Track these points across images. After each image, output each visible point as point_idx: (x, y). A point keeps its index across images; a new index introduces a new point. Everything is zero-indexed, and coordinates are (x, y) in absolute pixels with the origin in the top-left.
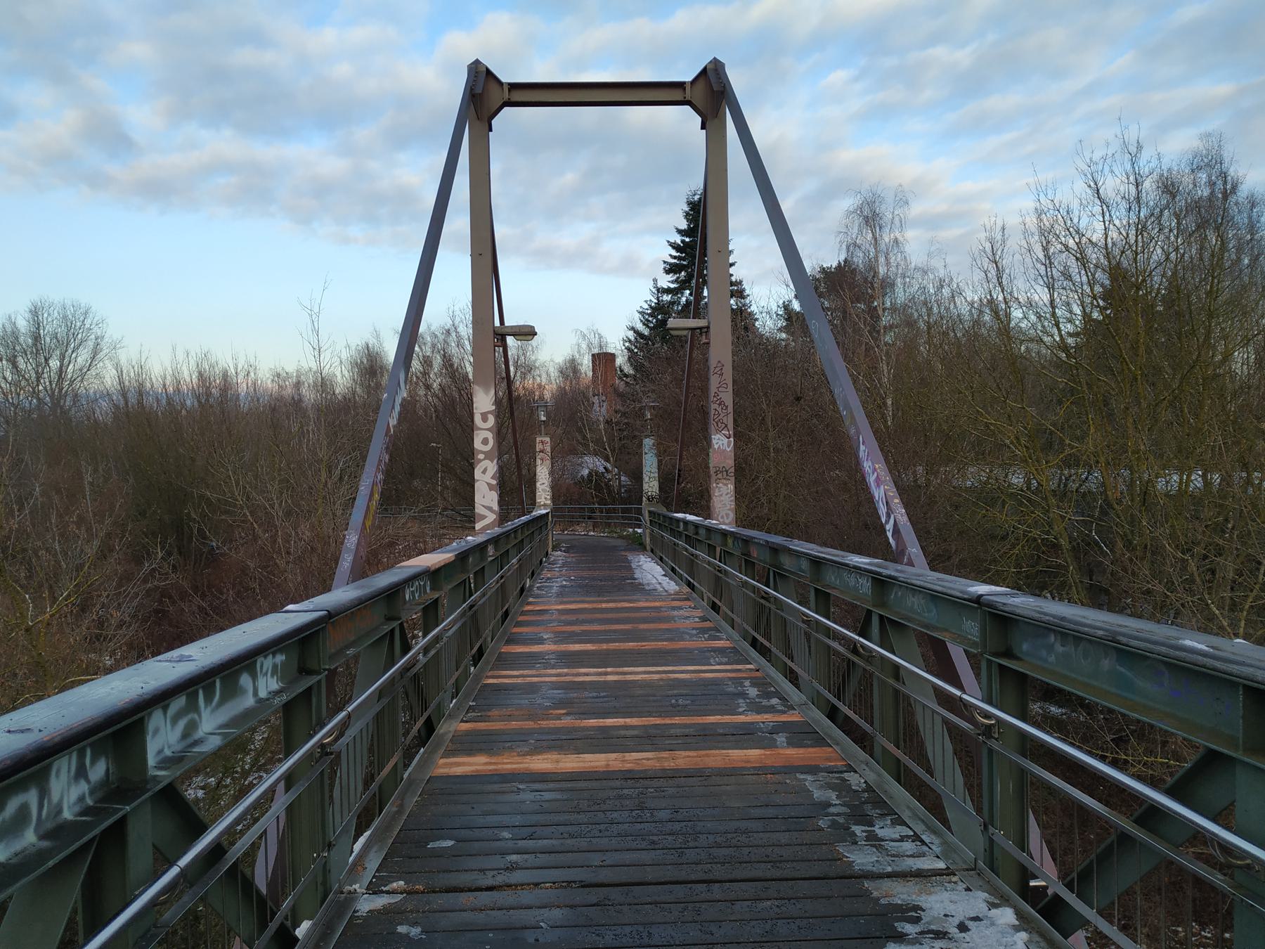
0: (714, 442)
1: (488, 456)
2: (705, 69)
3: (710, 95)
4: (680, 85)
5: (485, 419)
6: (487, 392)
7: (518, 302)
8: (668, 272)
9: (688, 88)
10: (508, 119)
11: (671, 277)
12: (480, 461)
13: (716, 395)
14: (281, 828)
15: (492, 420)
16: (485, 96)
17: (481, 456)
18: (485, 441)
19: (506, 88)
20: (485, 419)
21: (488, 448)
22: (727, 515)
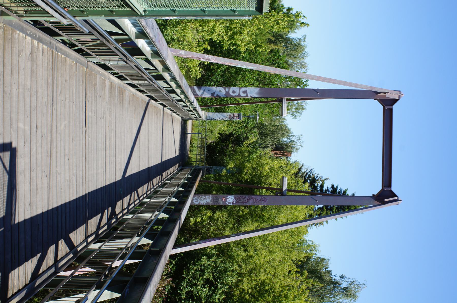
0: (231, 196)
1: (227, 93)
2: (189, 85)
3: (385, 196)
4: (390, 186)
5: (245, 92)
6: (257, 94)
7: (311, 105)
8: (333, 186)
9: (389, 189)
10: (379, 108)
11: (330, 186)
12: (225, 89)
13: (252, 198)
14: (181, 226)
15: (243, 95)
16: (388, 104)
17: (227, 90)
18: (234, 92)
19: (390, 107)
20: (245, 92)
21: (231, 93)
22: (197, 201)
